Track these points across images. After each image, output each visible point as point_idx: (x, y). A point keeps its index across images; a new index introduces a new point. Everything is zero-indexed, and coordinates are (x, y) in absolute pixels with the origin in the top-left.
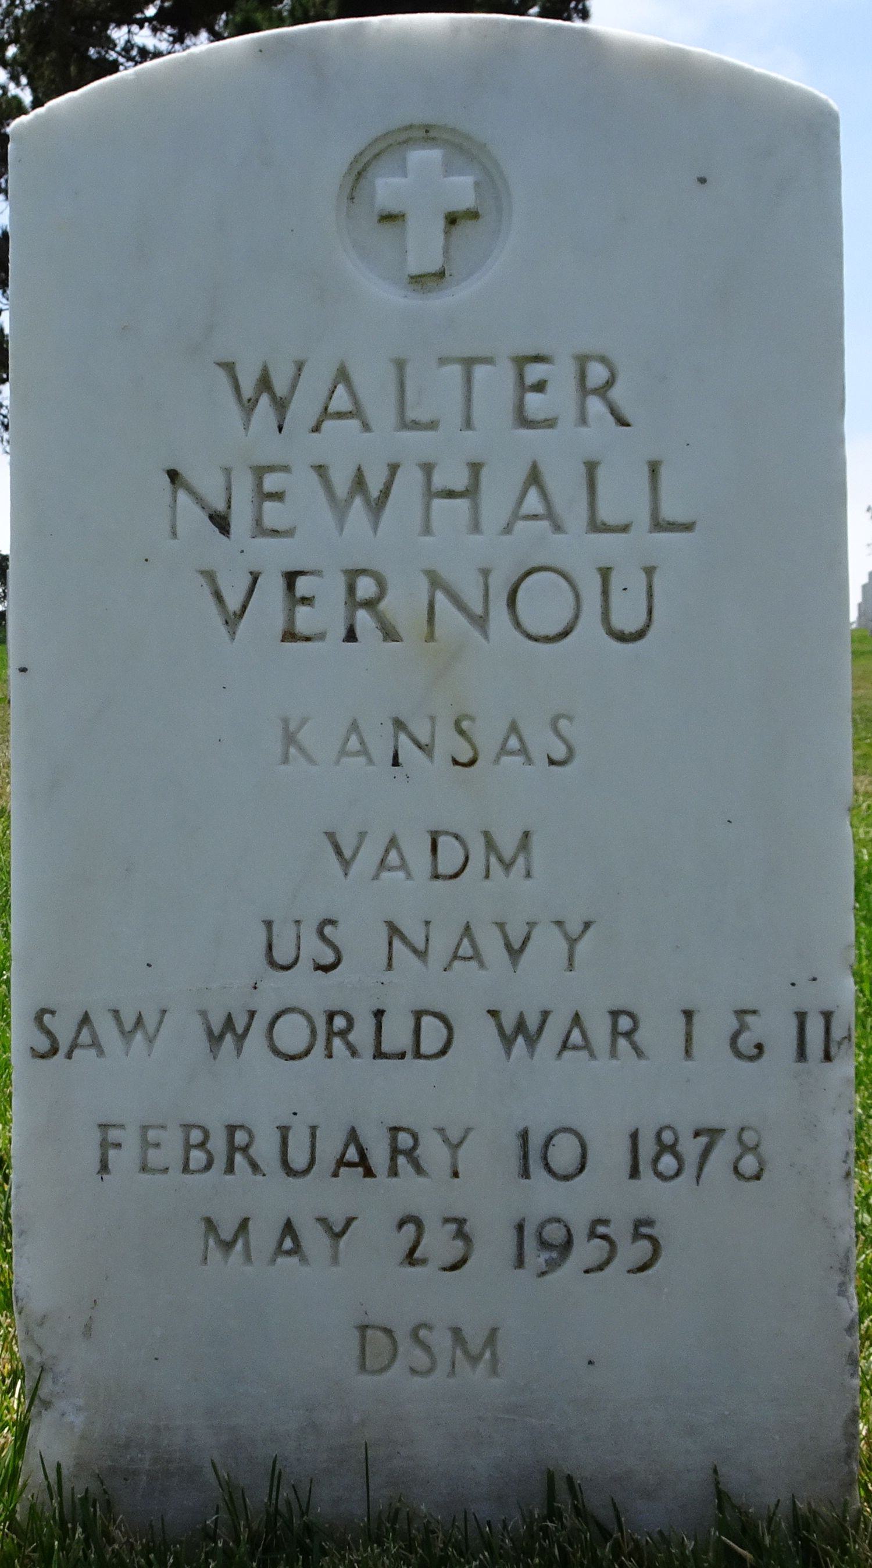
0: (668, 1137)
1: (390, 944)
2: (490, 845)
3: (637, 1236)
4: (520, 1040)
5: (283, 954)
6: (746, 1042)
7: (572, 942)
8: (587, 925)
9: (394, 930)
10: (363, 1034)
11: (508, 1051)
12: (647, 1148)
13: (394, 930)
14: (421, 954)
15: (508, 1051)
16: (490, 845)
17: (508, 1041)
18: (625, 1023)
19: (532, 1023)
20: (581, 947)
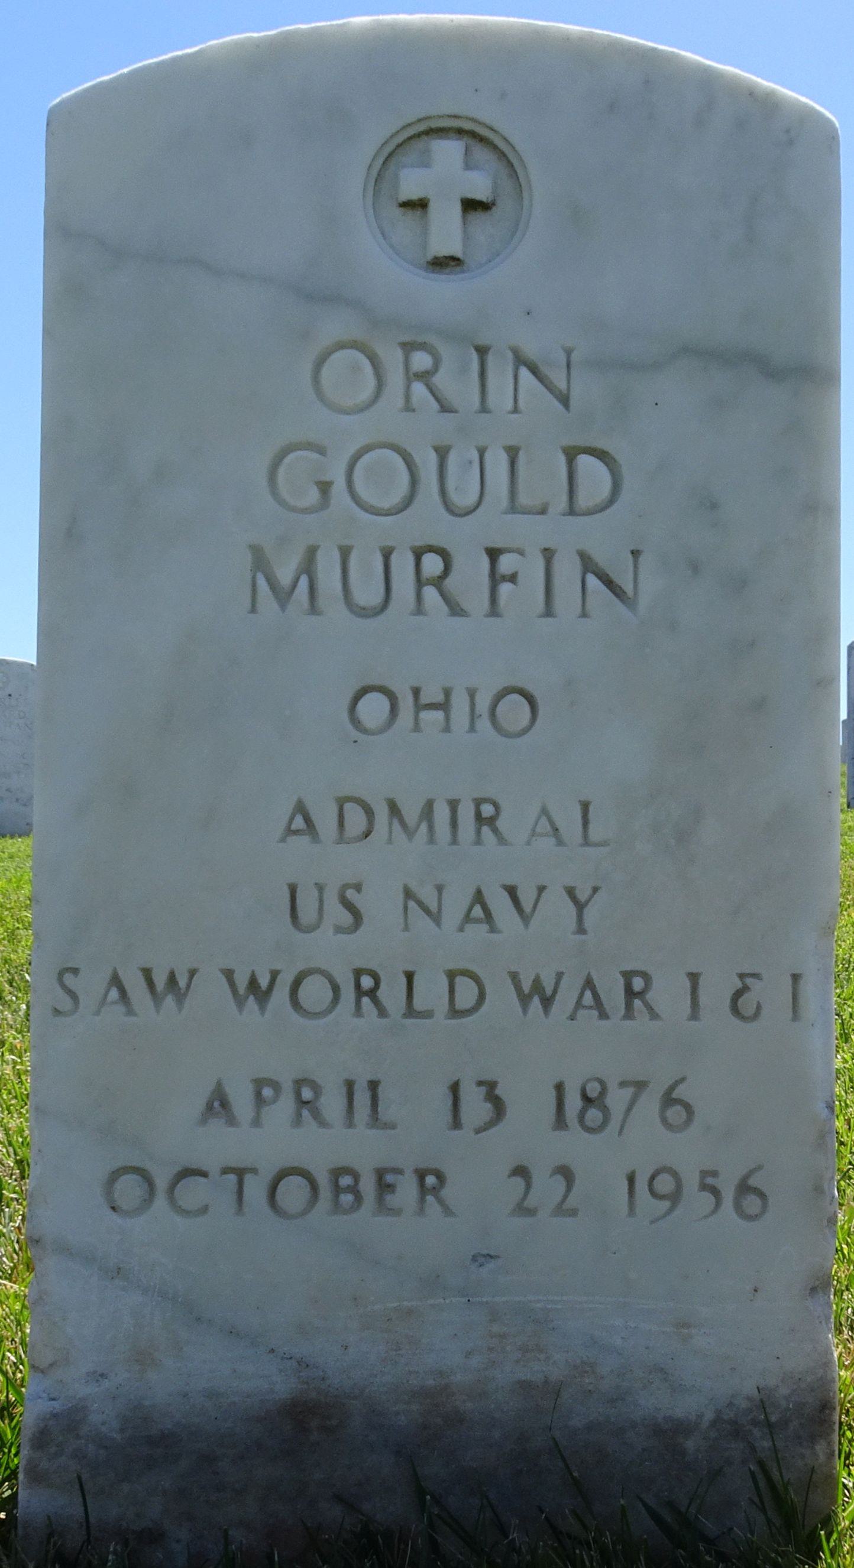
0: (593, 1090)
1: (406, 908)
2: (394, 809)
3: (704, 1187)
4: (536, 1000)
5: (307, 911)
6: (747, 1005)
7: (580, 907)
8: (595, 890)
9: (408, 894)
10: (392, 994)
11: (525, 1010)
12: (573, 1103)
13: (408, 894)
14: (436, 917)
15: (525, 1010)
16: (394, 809)
17: (524, 1000)
18: (367, 982)
19: (264, 982)
20: (591, 914)
